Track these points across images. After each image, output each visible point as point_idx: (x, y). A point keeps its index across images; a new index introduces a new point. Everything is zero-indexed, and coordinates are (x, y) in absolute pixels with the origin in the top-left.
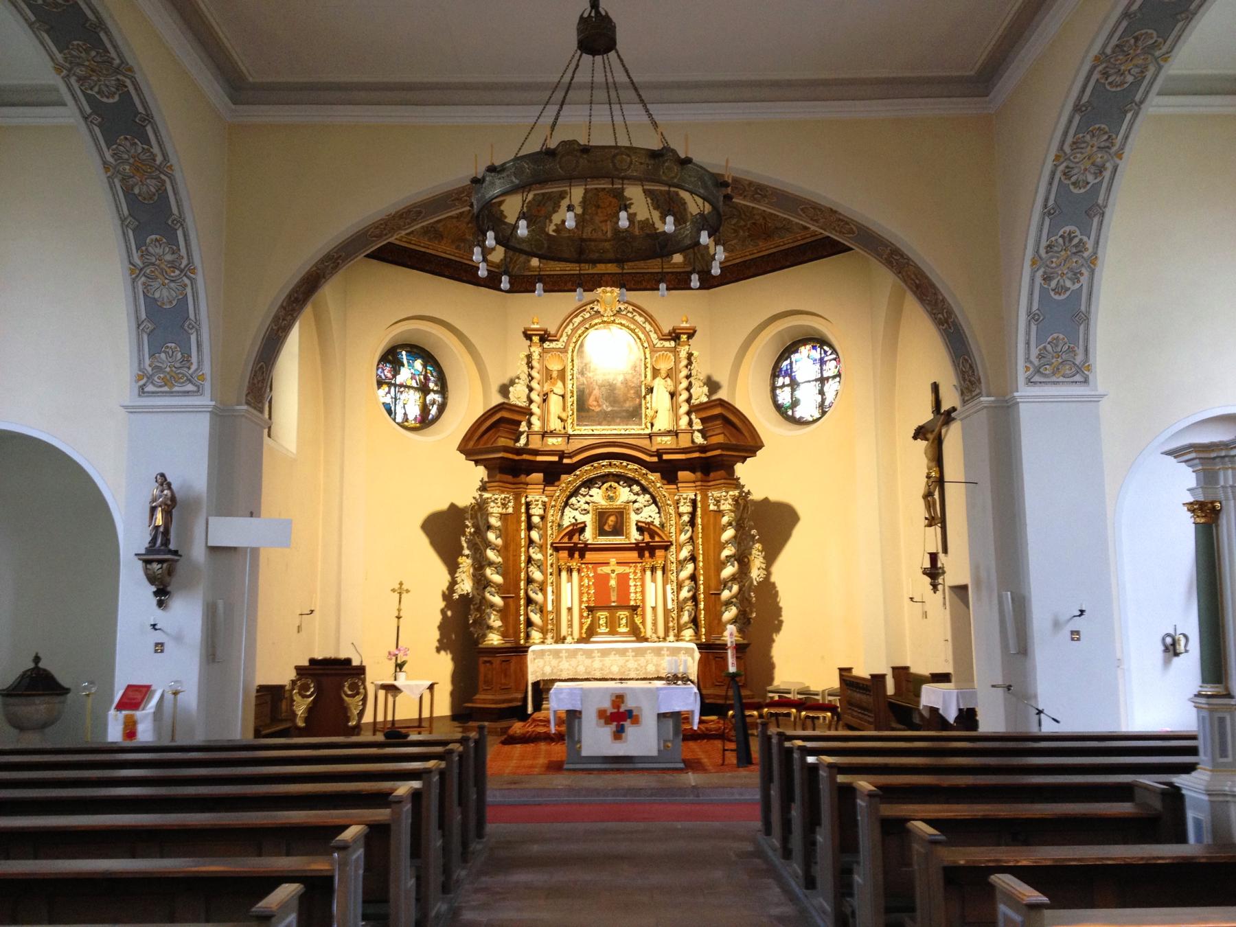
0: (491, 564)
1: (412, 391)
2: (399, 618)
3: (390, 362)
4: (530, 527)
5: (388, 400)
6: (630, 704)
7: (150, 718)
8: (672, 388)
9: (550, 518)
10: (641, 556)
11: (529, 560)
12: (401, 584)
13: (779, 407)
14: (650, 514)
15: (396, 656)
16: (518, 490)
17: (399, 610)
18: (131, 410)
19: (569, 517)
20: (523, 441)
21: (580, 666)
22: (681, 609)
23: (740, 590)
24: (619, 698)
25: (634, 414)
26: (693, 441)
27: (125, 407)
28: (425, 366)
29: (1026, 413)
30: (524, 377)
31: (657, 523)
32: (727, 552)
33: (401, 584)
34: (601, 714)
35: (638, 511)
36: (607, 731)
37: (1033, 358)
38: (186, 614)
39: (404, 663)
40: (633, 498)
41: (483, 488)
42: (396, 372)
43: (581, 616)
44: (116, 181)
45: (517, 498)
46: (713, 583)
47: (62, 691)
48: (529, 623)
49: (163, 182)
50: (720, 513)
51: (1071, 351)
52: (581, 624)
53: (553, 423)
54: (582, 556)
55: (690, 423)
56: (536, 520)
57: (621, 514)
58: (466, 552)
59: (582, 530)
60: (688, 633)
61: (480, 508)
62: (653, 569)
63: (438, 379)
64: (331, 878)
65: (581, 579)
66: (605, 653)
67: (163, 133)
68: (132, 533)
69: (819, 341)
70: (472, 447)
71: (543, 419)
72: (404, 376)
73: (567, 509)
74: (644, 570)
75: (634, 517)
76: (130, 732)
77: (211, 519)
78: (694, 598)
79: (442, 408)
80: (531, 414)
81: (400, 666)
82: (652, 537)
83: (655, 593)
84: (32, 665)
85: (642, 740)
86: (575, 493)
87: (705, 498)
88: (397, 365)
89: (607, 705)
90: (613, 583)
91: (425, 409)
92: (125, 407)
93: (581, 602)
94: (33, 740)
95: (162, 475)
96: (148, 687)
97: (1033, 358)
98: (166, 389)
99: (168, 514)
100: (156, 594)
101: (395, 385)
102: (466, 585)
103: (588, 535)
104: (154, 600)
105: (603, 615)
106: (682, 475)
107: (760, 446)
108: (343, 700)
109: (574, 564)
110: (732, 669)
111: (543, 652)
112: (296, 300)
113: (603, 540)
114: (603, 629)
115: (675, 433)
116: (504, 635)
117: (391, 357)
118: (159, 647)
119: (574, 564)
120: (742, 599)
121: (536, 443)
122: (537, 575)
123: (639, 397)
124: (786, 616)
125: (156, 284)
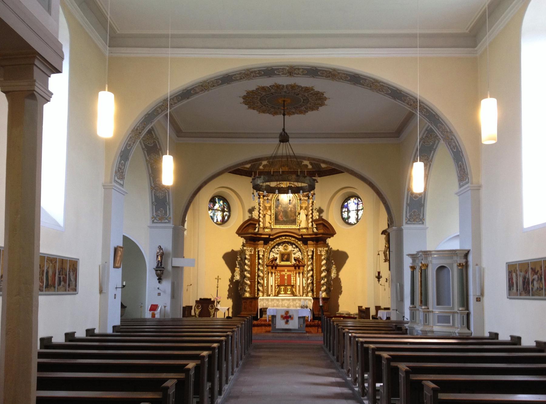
0: (246, 270)
4: (259, 258)
5: (211, 215)
6: (290, 314)
8: (306, 213)
9: (266, 256)
10: (295, 268)
11: (259, 269)
13: (344, 219)
14: (298, 255)
16: (255, 247)
18: (150, 227)
19: (272, 255)
20: (257, 230)
21: (275, 303)
22: (308, 286)
23: (328, 281)
24: (287, 312)
25: (294, 222)
26: (313, 231)
28: (223, 203)
29: (405, 232)
30: (257, 209)
31: (301, 258)
32: (323, 268)
34: (282, 316)
35: (294, 254)
36: (283, 322)
37: (408, 216)
38: (166, 285)
40: (293, 249)
41: (244, 245)
42: (214, 205)
43: (275, 288)
45: (255, 250)
46: (318, 278)
48: (258, 290)
50: (321, 255)
51: (419, 215)
52: (275, 291)
53: (268, 224)
54: (276, 268)
55: (312, 225)
56: (261, 256)
57: (289, 255)
58: (238, 266)
59: (276, 260)
60: (310, 294)
61: (242, 252)
62: (299, 273)
63: (228, 207)
65: (275, 276)
66: (283, 300)
68: (150, 262)
69: (357, 197)
70: (241, 232)
71: (264, 223)
72: (217, 206)
73: (271, 253)
74: (296, 273)
75: (293, 256)
76: (153, 315)
77: (173, 259)
78: (312, 283)
79: (229, 217)
80: (260, 221)
82: (299, 262)
83: (299, 281)
85: (294, 324)
86: (274, 247)
87: (317, 250)
89: (283, 314)
90: (286, 277)
91: (223, 217)
93: (275, 283)
97: (408, 216)
99: (162, 257)
102: (237, 277)
103: (278, 261)
104: (158, 281)
105: (282, 288)
106: (309, 242)
107: (335, 233)
109: (273, 271)
110: (321, 304)
111: (263, 299)
113: (283, 263)
114: (282, 292)
115: (307, 228)
116: (250, 293)
117: (213, 201)
118: (159, 294)
119: (273, 271)
120: (328, 284)
121: (261, 231)
122: (261, 274)
123: (296, 215)
124: (343, 289)
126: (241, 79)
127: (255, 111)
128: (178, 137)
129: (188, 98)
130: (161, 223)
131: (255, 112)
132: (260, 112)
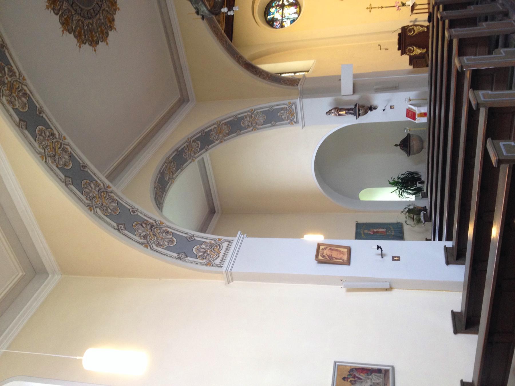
1: (284, 12)
2: (382, 8)
3: (273, 23)
7: (419, 108)
12: (367, 8)
15: (399, 6)
17: (379, 8)
18: (304, 125)
27: (303, 128)
28: (273, 7)
33: (367, 8)
38: (379, 99)
39: (402, 3)
42: (277, 20)
44: (225, 138)
47: (409, 136)
49: (223, 124)
64: (473, 70)
67: (206, 126)
68: (349, 120)
76: (425, 114)
77: (342, 94)
81: (403, 5)
84: (399, 147)
88: (274, 20)
92: (303, 128)
94: (426, 145)
95: (327, 113)
96: (407, 110)
98: (295, 115)
99: (341, 110)
100: (371, 110)
101: (282, 19)
104: (374, 111)
108: (416, 35)
112: (256, 71)
117: (271, 23)
118: (392, 107)
125: (258, 122)
126: (25, 94)
127: (116, 17)
128: (188, 101)
129: (84, 167)
130: (296, 113)
131: (117, 17)
132: (115, 10)
